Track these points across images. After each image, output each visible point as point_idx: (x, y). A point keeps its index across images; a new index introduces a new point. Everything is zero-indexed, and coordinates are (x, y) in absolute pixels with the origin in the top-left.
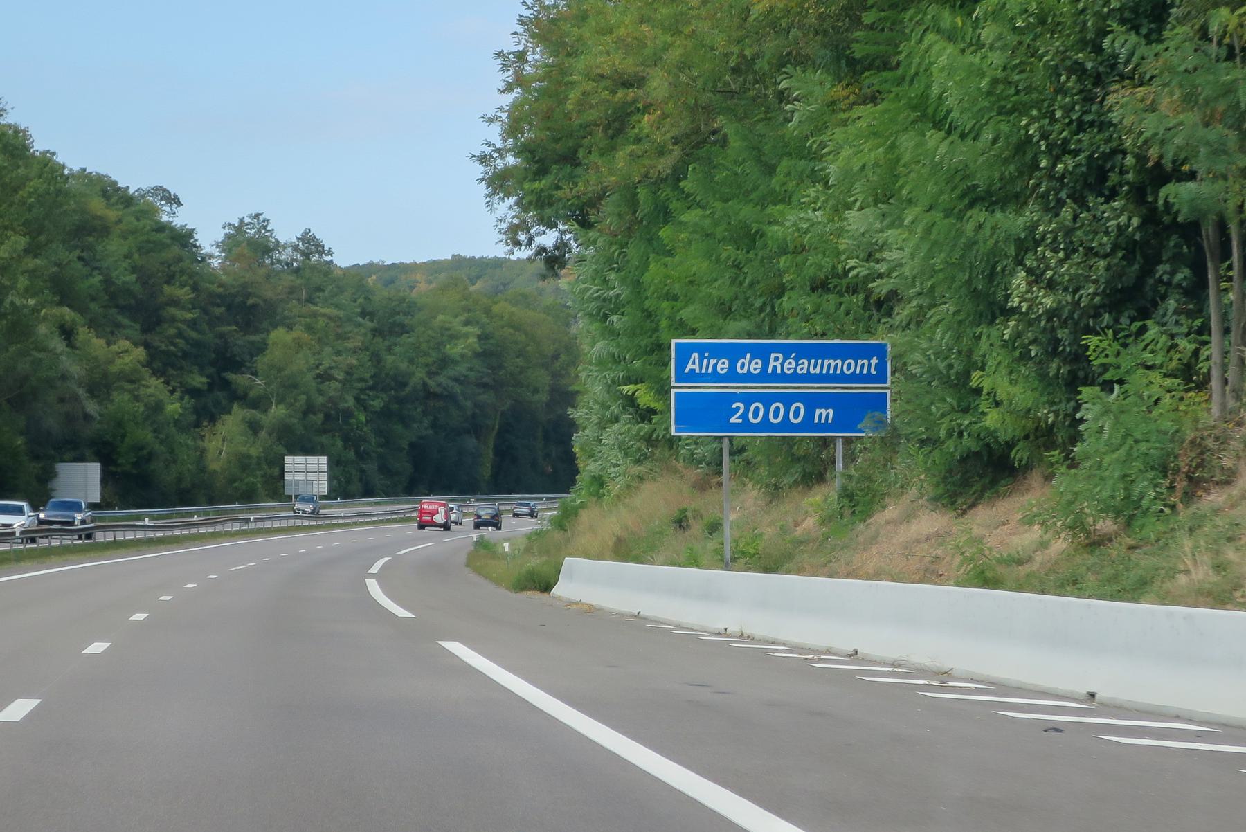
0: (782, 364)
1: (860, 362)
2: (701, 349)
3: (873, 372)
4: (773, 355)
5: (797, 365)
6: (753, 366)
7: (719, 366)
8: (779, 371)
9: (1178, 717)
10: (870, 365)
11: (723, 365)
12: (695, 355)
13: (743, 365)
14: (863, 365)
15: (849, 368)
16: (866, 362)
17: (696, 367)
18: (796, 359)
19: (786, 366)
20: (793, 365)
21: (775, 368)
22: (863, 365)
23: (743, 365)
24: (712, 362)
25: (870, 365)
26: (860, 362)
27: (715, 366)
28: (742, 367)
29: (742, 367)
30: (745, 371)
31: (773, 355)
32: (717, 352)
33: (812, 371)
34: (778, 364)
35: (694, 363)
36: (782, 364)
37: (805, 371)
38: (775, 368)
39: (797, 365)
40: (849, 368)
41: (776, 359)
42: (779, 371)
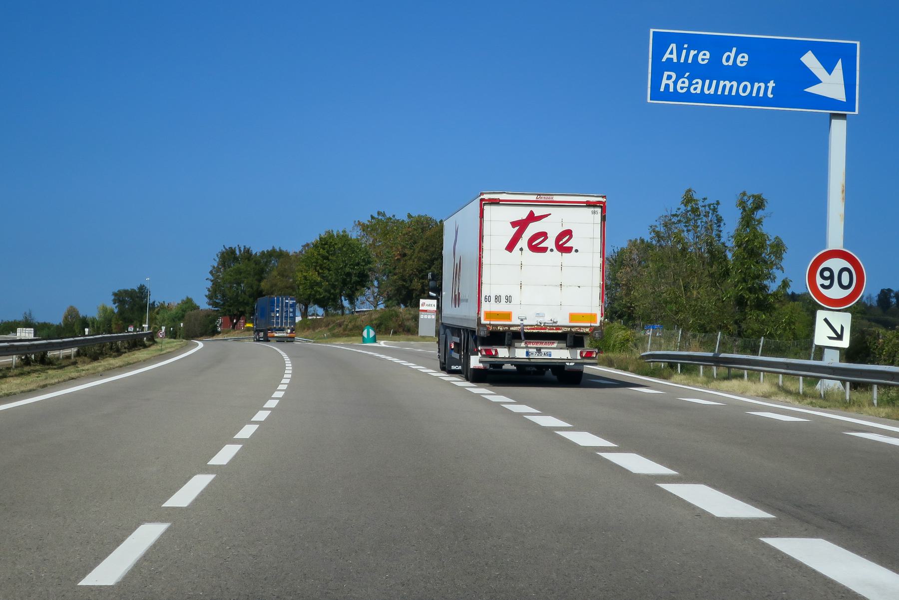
0: (675, 83)
1: (756, 85)
2: (680, 40)
3: (771, 96)
4: (666, 74)
5: (690, 84)
6: (739, 59)
7: (701, 56)
8: (671, 90)
9: (8, 395)
10: (766, 88)
11: (704, 57)
12: (673, 46)
13: (728, 58)
14: (759, 88)
15: (745, 87)
16: (762, 85)
17: (674, 57)
18: (690, 79)
19: (679, 85)
20: (687, 85)
21: (667, 86)
22: (759, 88)
23: (728, 58)
24: (693, 53)
25: (766, 88)
26: (756, 85)
27: (696, 56)
28: (728, 60)
29: (728, 60)
30: (730, 63)
31: (666, 74)
32: (697, 43)
33: (706, 92)
34: (671, 82)
35: (671, 53)
36: (675, 83)
37: (698, 91)
38: (667, 86)
39: (690, 84)
40: (745, 87)
41: (669, 77)
42: (671, 90)
